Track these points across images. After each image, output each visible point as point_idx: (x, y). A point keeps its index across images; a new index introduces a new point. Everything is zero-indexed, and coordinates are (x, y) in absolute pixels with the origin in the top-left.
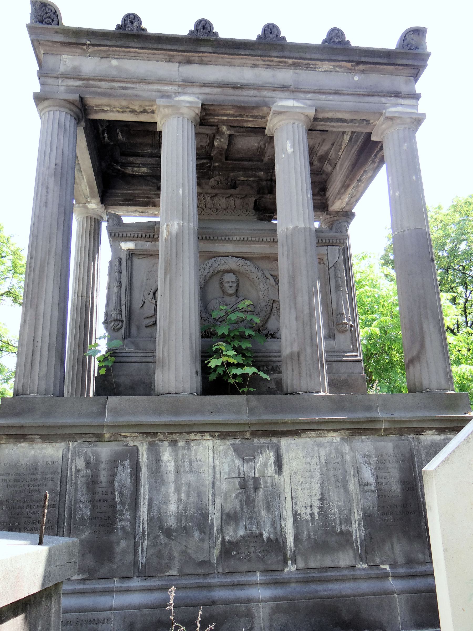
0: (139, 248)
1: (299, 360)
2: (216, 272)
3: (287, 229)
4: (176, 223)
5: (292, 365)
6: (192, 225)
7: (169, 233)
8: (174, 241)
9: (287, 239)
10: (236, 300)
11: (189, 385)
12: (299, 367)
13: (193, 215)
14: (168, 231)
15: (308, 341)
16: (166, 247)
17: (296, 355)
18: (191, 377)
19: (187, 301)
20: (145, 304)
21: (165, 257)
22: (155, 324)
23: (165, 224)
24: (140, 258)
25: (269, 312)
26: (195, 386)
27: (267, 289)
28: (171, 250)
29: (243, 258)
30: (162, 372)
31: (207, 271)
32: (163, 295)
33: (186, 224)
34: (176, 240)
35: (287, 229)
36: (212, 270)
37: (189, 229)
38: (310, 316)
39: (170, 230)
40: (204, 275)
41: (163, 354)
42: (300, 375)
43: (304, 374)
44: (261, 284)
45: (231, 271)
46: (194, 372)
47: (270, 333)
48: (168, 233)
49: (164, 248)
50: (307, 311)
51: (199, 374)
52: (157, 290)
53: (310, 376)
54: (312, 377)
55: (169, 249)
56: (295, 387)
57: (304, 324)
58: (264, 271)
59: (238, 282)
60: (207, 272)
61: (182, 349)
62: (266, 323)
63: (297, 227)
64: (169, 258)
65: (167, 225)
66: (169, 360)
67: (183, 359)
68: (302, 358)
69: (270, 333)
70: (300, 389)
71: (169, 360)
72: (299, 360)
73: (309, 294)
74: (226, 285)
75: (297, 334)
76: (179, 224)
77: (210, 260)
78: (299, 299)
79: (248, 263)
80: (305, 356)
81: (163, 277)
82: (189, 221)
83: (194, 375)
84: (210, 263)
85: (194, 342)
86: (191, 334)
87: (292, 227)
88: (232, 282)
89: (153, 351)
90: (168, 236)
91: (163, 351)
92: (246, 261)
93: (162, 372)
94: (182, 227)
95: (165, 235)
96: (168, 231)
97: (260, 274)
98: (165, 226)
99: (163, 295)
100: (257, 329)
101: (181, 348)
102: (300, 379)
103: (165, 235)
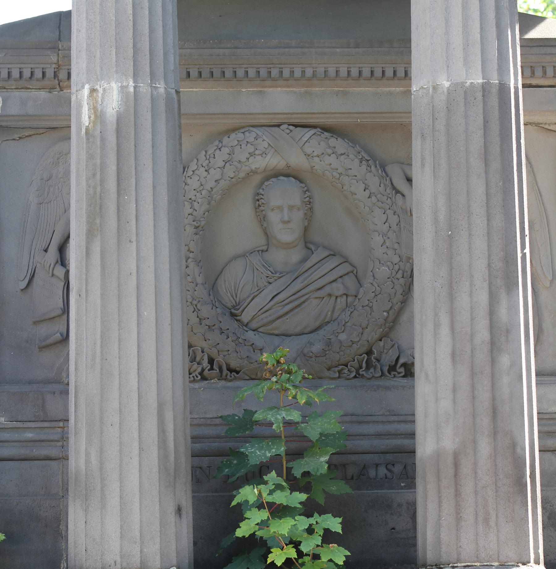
0: (14, 110)
1: (456, 475)
2: (242, 175)
3: (435, 88)
4: (115, 86)
5: (439, 487)
6: (161, 87)
7: (98, 116)
8: (112, 139)
9: (434, 119)
10: (304, 260)
11: (158, 546)
12: (457, 494)
13: (165, 54)
14: (95, 108)
15: (485, 422)
16: (91, 157)
17: (450, 460)
18: (163, 524)
19: (149, 313)
20: (35, 279)
21: (88, 186)
22: (66, 338)
23: (87, 87)
24: (16, 136)
25: (399, 297)
26: (174, 547)
27: (394, 227)
28: (103, 167)
29: (325, 129)
30: (86, 511)
31: (215, 174)
32: (83, 294)
33: (144, 88)
34: (118, 137)
35: (435, 88)
36: (230, 172)
37: (153, 100)
38: (492, 351)
39: (99, 108)
40: (208, 187)
41: (88, 462)
42: (459, 519)
43: (468, 514)
44: (378, 212)
45: (289, 174)
46: (171, 509)
47: (402, 361)
48: (95, 112)
49: (84, 156)
50: (483, 334)
51: (184, 513)
52: (69, 237)
53: (486, 520)
54: (492, 523)
55: (98, 162)
56: (444, 548)
57: (473, 374)
58: (389, 168)
59: (309, 203)
60: (218, 177)
61: (136, 451)
62: (391, 328)
63: (463, 84)
64: (99, 189)
65: (93, 91)
66: (103, 479)
67: (140, 477)
68: (466, 469)
69: (402, 361)
70: (459, 554)
71: (103, 479)
72: (456, 475)
73: (490, 284)
74: (274, 218)
75: (454, 401)
76: (123, 88)
77: (226, 140)
78: (463, 301)
79: (340, 145)
80: (475, 464)
81: (84, 243)
82: (153, 76)
83: (172, 518)
84: (226, 150)
85: (170, 427)
86: (161, 407)
87: (447, 84)
88: (291, 208)
89: (61, 424)
90: (95, 122)
91: (88, 454)
92: (333, 141)
93: (86, 511)
94: (132, 98)
95: (86, 120)
96: (95, 108)
97: (374, 181)
98: (86, 91)
99: (83, 294)
100: (364, 349)
101: (136, 444)
102: (458, 528)
103: (86, 120)
